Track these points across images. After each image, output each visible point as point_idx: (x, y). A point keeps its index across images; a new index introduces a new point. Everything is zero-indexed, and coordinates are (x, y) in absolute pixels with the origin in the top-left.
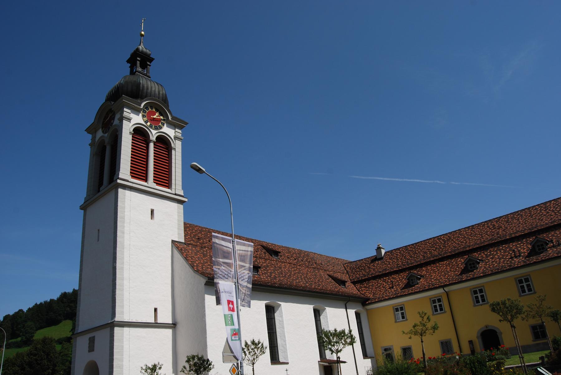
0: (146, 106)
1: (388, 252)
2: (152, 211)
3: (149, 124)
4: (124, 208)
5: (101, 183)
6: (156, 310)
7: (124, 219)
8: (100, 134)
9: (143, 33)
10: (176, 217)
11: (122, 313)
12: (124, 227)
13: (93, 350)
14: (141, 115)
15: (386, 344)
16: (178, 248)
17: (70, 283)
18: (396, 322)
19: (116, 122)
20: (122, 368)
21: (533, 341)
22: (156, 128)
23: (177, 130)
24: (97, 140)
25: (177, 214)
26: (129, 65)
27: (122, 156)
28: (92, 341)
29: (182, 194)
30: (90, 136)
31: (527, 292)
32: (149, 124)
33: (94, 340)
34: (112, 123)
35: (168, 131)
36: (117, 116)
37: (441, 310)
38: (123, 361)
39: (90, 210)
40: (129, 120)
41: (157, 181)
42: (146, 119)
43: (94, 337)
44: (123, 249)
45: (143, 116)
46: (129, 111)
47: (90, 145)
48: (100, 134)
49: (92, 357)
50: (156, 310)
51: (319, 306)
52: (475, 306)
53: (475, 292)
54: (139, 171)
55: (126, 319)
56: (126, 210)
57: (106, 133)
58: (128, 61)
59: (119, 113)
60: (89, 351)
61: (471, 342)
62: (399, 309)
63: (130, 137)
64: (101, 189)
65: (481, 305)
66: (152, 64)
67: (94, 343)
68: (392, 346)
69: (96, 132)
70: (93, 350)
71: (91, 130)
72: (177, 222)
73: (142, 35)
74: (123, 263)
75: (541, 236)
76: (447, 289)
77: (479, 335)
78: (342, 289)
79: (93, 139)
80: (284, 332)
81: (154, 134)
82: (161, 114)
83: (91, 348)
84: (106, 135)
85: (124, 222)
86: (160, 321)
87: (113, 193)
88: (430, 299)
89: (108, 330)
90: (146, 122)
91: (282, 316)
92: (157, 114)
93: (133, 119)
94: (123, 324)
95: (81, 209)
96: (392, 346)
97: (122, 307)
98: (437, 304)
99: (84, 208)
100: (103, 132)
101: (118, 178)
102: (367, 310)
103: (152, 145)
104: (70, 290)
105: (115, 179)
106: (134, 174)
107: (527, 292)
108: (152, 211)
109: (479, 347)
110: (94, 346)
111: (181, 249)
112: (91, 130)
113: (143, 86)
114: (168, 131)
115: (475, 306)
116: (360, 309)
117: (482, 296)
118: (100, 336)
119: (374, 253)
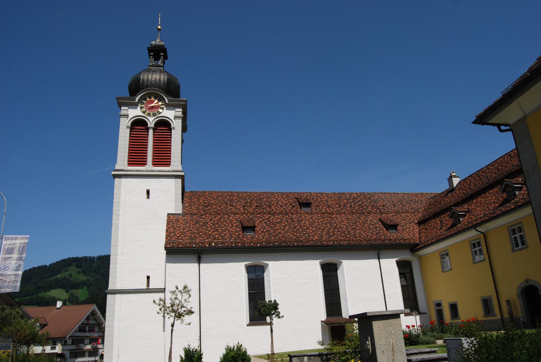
0: (143, 98)
1: (465, 179)
2: (148, 192)
4: (120, 194)
6: (148, 278)
7: (119, 203)
9: (159, 27)
10: (173, 191)
12: (119, 210)
14: (139, 108)
15: (437, 298)
18: (443, 272)
22: (154, 115)
23: (177, 110)
25: (174, 188)
29: (181, 169)
31: (521, 247)
35: (169, 114)
37: (523, 243)
38: (114, 322)
40: (127, 116)
44: (118, 229)
45: (141, 108)
46: (127, 108)
50: (148, 278)
51: (330, 258)
52: (513, 251)
54: (137, 157)
55: (118, 287)
56: (121, 196)
61: (508, 302)
62: (444, 255)
63: (128, 130)
65: (520, 250)
68: (441, 300)
73: (159, 30)
74: (117, 241)
76: (482, 229)
78: (392, 235)
80: (270, 291)
81: (151, 121)
82: (159, 100)
85: (119, 206)
86: (151, 287)
88: (470, 242)
90: (144, 112)
91: (269, 276)
92: (156, 102)
94: (379, 261)
96: (441, 300)
97: (115, 277)
102: (420, 257)
103: (151, 132)
108: (148, 192)
113: (143, 80)
114: (169, 114)
115: (513, 251)
116: (406, 256)
117: (521, 237)
119: (447, 187)
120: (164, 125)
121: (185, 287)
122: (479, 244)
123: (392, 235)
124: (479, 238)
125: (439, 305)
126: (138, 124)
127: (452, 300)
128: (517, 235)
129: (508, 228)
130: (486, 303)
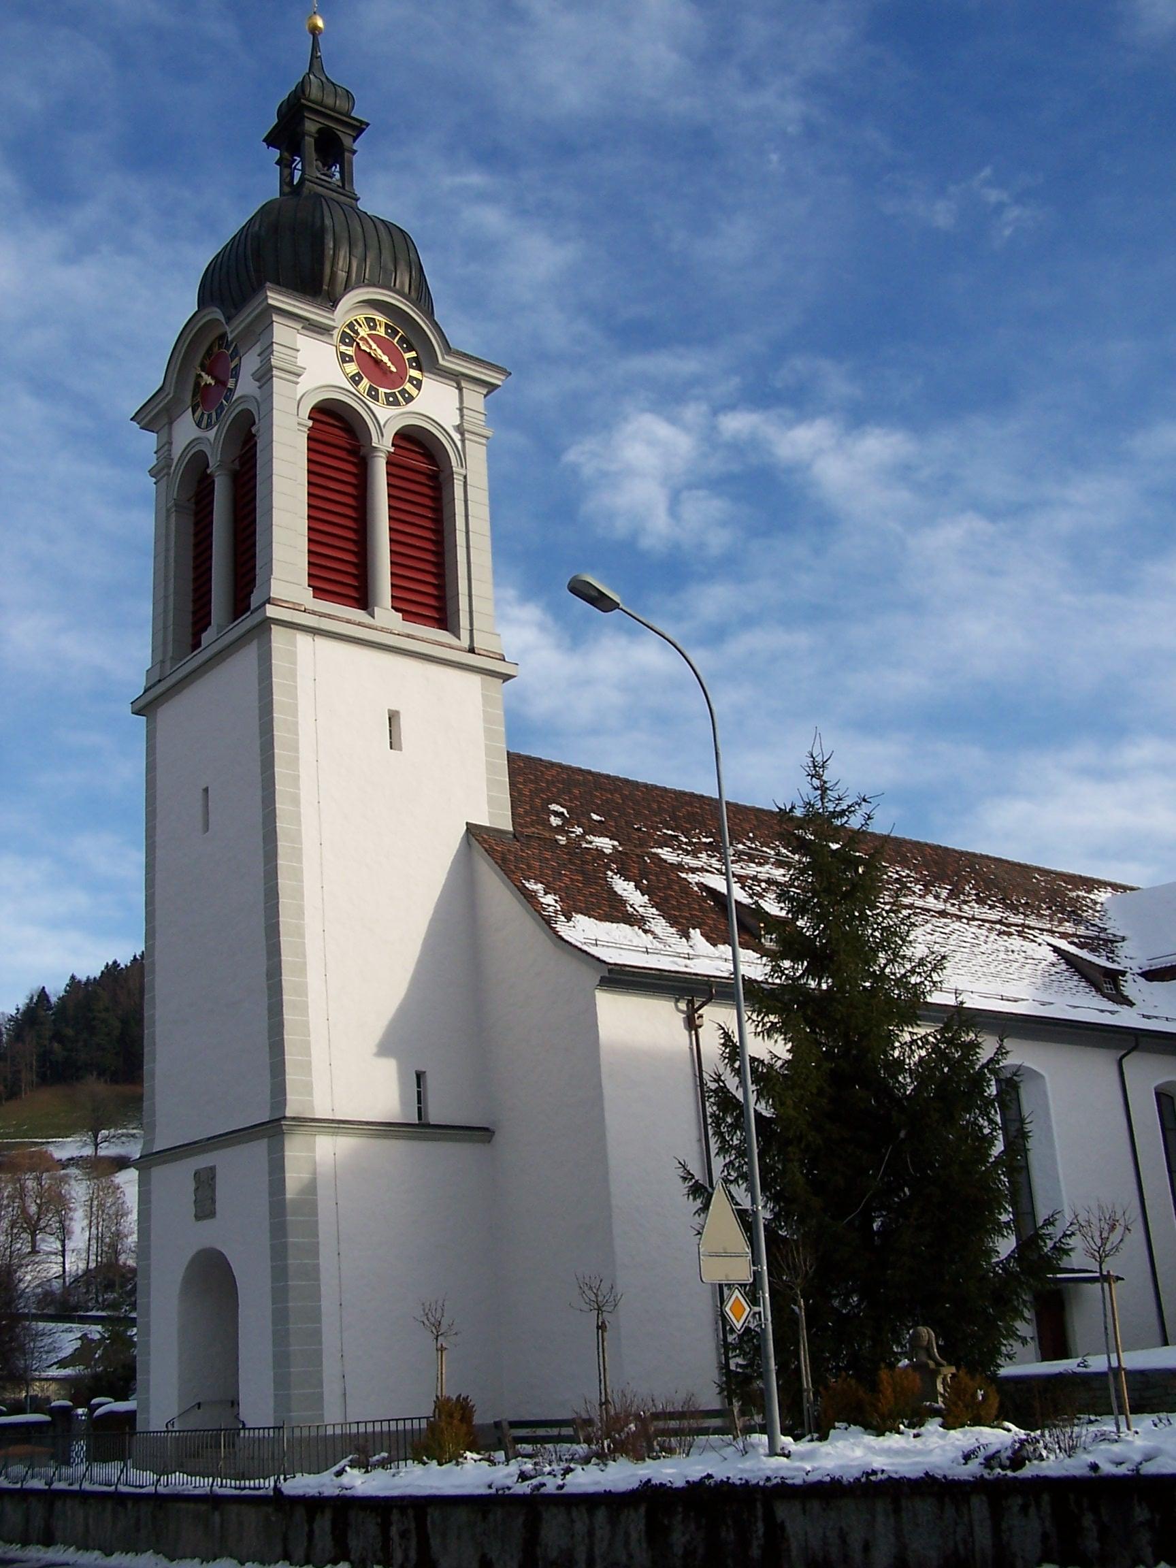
5: (201, 620)
8: (186, 430)
11: (308, 1088)
13: (212, 1214)
16: (490, 852)
17: (124, 952)
19: (245, 386)
20: (318, 1279)
22: (393, 402)
24: (177, 451)
26: (276, 154)
27: (278, 451)
28: (205, 1182)
30: (150, 440)
32: (365, 383)
33: (213, 1178)
34: (232, 391)
36: (250, 363)
39: (167, 714)
41: (405, 606)
42: (352, 368)
43: (212, 1169)
47: (153, 473)
48: (186, 430)
49: (208, 1235)
54: (341, 574)
55: (321, 1110)
57: (209, 426)
59: (257, 349)
60: (198, 1217)
64: (206, 637)
66: (355, 158)
67: (213, 1189)
70: (212, 1214)
79: (164, 449)
81: (384, 421)
83: (205, 1208)
84: (211, 434)
87: (247, 657)
89: (259, 1149)
90: (355, 379)
93: (309, 364)
95: (137, 712)
99: (146, 707)
100: (199, 425)
101: (269, 601)
104: (124, 961)
105: (255, 601)
110: (213, 1201)
111: (504, 859)
112: (155, 415)
118: (238, 1170)
120: (422, 454)
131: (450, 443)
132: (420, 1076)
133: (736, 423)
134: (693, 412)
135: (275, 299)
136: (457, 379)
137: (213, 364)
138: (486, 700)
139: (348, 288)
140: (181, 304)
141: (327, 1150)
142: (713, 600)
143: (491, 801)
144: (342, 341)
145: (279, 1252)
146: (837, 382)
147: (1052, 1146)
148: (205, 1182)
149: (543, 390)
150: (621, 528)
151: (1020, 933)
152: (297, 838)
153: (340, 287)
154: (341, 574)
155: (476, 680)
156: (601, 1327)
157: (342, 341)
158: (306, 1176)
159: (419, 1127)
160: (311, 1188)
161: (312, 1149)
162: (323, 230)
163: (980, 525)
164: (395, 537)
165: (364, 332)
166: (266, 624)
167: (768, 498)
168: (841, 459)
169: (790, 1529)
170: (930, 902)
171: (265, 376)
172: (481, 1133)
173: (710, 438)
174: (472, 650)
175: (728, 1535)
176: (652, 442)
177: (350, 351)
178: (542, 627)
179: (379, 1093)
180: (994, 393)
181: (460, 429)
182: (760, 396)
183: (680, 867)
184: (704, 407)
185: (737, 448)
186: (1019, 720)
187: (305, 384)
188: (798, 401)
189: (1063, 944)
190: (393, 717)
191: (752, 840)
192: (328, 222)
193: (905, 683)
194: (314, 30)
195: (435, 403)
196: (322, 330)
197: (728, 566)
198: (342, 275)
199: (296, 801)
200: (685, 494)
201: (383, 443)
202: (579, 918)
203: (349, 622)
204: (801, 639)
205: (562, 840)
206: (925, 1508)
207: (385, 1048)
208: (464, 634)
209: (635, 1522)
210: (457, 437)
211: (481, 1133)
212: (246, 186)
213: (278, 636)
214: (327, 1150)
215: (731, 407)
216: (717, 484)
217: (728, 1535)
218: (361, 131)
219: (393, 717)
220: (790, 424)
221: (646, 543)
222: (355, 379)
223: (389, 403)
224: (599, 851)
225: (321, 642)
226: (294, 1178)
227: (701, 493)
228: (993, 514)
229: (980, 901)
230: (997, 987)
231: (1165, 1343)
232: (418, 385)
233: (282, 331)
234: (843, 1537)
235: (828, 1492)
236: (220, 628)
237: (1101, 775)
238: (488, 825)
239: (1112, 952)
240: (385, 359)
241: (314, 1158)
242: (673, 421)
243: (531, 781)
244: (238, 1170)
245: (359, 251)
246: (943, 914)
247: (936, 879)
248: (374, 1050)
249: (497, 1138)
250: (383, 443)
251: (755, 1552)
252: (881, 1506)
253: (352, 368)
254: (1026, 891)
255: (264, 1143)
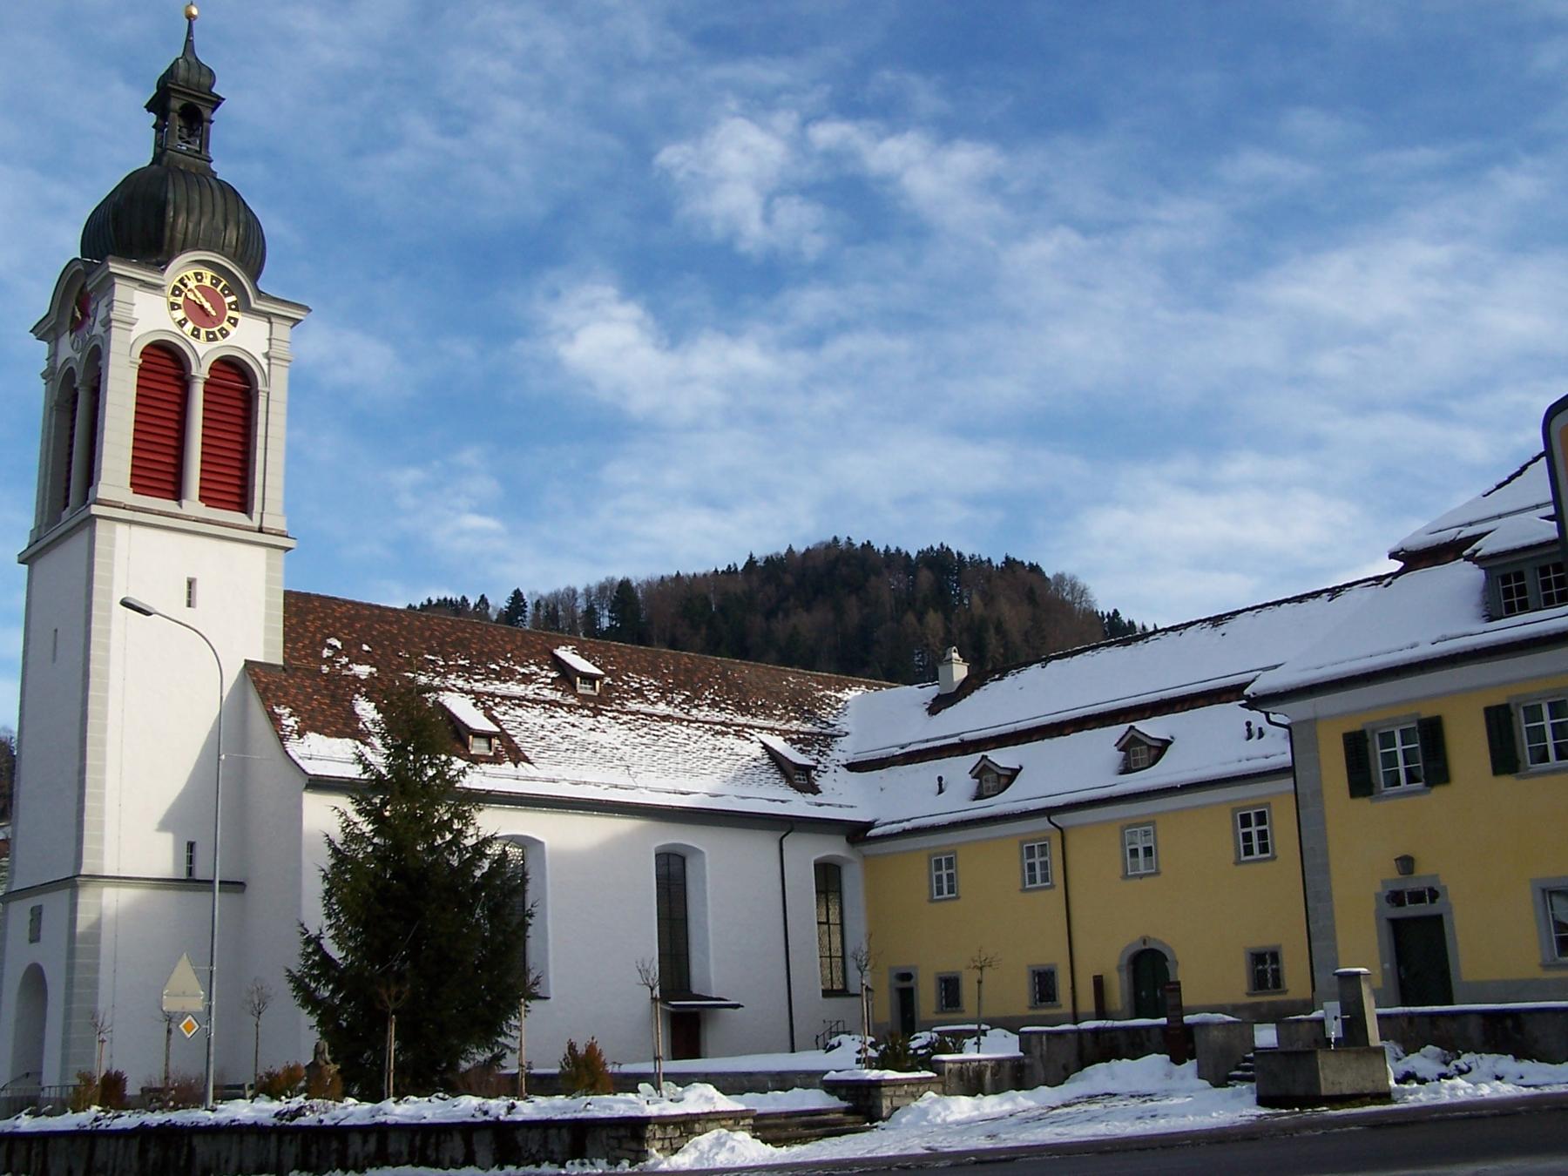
3: (190, 326)
11: (100, 854)
16: (257, 683)
18: (1125, 876)
19: (98, 329)
21: (1248, 994)
22: (211, 338)
28: (37, 913)
31: (1257, 854)
32: (190, 326)
37: (1264, 848)
39: (43, 564)
42: (180, 314)
47: (44, 375)
49: (36, 954)
52: (1238, 862)
53: (1245, 821)
54: (158, 473)
58: (150, 107)
60: (31, 941)
61: (1099, 982)
69: (57, 339)
71: (45, 330)
72: (263, 609)
75: (1141, 726)
77: (1125, 962)
79: (53, 356)
81: (203, 354)
83: (35, 937)
98: (1254, 830)
106: (140, 483)
107: (1257, 854)
109: (1118, 993)
112: (45, 330)
115: (1238, 862)
117: (1263, 835)
120: (235, 379)
121: (1250, 737)
122: (1044, 850)
123: (798, 805)
124: (1047, 839)
125: (906, 977)
126: (164, 362)
127: (947, 967)
128: (1254, 830)
129: (1234, 811)
130: (1264, 967)
131: (259, 366)
132: (191, 846)
133: (827, 134)
134: (785, 121)
135: (115, 267)
136: (268, 316)
137: (78, 303)
138: (270, 567)
139: (183, 250)
140: (70, 245)
141: (112, 900)
142: (812, 303)
143: (267, 643)
144: (173, 294)
145: (70, 968)
146: (925, 95)
147: (705, 905)
148: (37, 913)
149: (634, 95)
150: (718, 230)
151: (737, 734)
152: (105, 676)
153: (178, 244)
154: (158, 473)
155: (263, 550)
156: (169, 1031)
157: (173, 294)
158: (93, 916)
159: (189, 881)
160: (97, 926)
161: (100, 896)
162: (165, 203)
163: (1073, 239)
164: (205, 439)
165: (192, 284)
166: (93, 518)
167: (863, 210)
168: (930, 171)
169: (198, 1150)
170: (661, 708)
171: (107, 323)
172: (235, 886)
173: (799, 144)
174: (261, 530)
175: (172, 1154)
176: (745, 149)
177: (180, 300)
178: (639, 324)
179: (161, 858)
180: (1082, 116)
181: (267, 356)
182: (848, 107)
183: (430, 688)
184: (795, 116)
185: (833, 157)
186: (1121, 432)
187: (137, 331)
188: (890, 114)
189: (777, 743)
190: (191, 583)
191: (507, 660)
192: (170, 196)
193: (1003, 391)
194: (190, 17)
195: (248, 337)
196: (157, 287)
197: (823, 271)
198: (179, 236)
199: (107, 648)
200: (778, 201)
201: (200, 371)
202: (312, 737)
203: (160, 513)
204: (901, 345)
205: (325, 669)
206: (251, 1140)
207: (164, 826)
208: (256, 517)
209: (135, 1144)
210: (264, 362)
211: (235, 886)
212: (132, 146)
213: (101, 528)
214: (112, 900)
215: (820, 118)
216: (808, 191)
217: (172, 1154)
218: (218, 104)
219: (191, 583)
220: (880, 138)
221: (743, 247)
222: (181, 324)
223: (209, 340)
224: (356, 677)
225: (135, 529)
226: (84, 919)
227: (795, 200)
228: (1085, 229)
229: (714, 705)
230: (668, 783)
231: (793, 1051)
232: (235, 322)
233: (121, 290)
234: (218, 1155)
235: (215, 1130)
236: (73, 511)
237: (1202, 487)
238: (262, 660)
239: (828, 746)
240: (207, 305)
241: (103, 905)
242: (765, 127)
243: (320, 619)
244: (53, 904)
245: (194, 218)
246: (666, 718)
247: (679, 686)
248: (156, 826)
249: (249, 890)
250: (200, 371)
251: (182, 1163)
252: (235, 1138)
253: (180, 314)
254: (770, 693)
255: (68, 891)
